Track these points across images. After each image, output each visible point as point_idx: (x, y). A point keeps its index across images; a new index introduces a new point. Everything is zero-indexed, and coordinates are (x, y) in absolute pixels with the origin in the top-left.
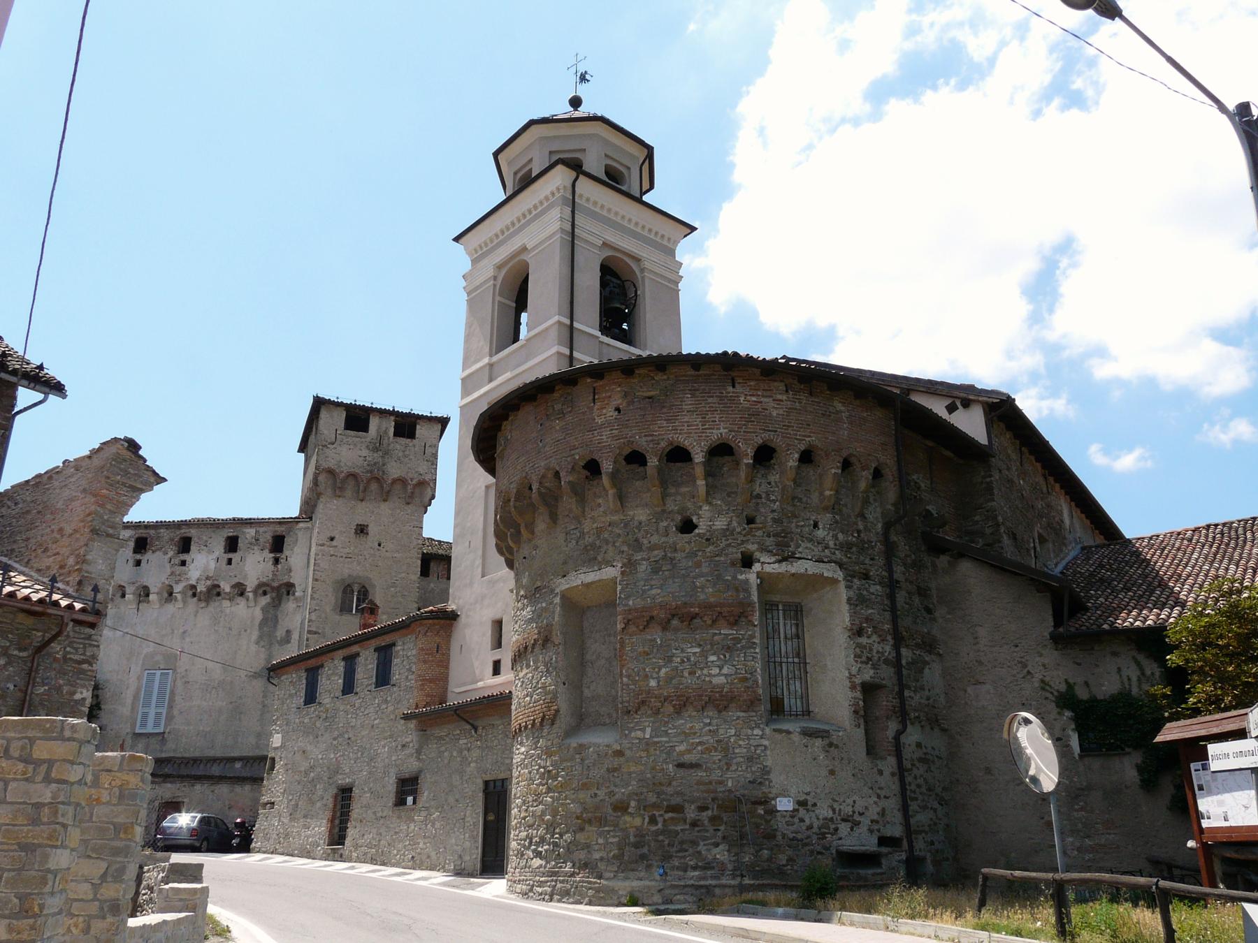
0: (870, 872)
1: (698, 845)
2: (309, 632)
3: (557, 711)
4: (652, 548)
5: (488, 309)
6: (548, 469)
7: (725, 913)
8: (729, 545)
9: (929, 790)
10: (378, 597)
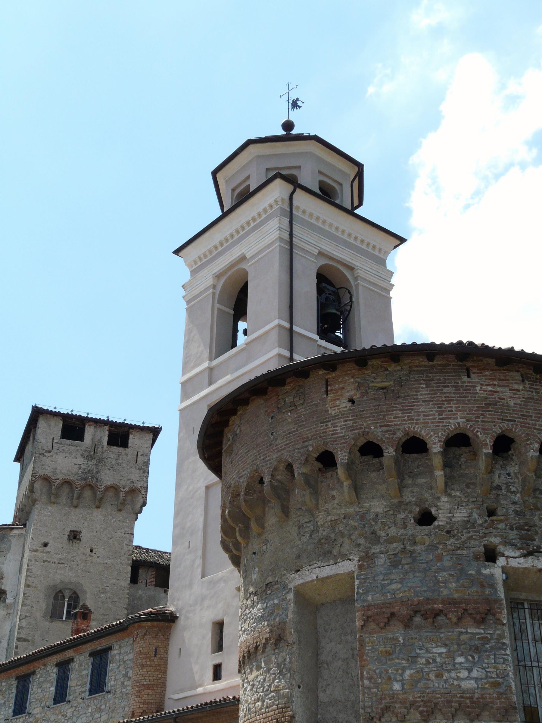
2: (19, 639)
4: (391, 540)
5: (207, 315)
6: (280, 462)
8: (470, 538)
10: (89, 600)
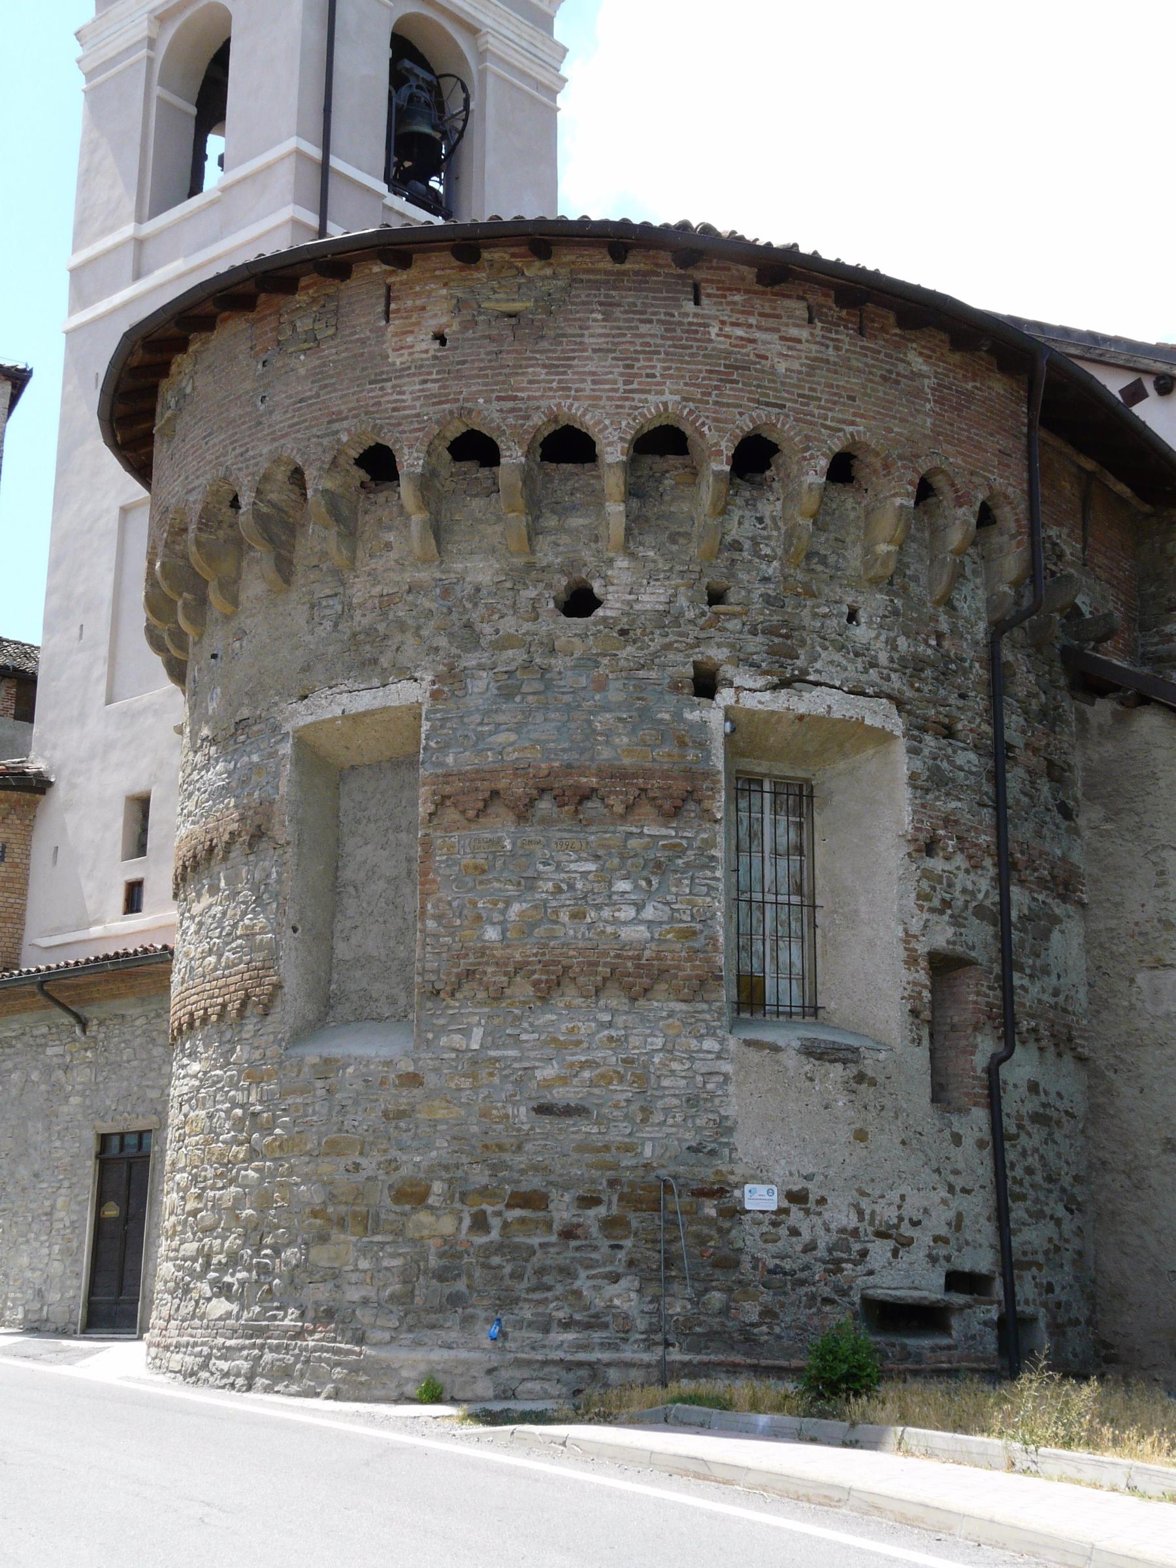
0: (927, 1342)
1: (575, 1277)
3: (278, 987)
4: (503, 643)
5: (133, 114)
6: (277, 461)
7: (635, 1422)
8: (667, 647)
9: (1050, 1179)
